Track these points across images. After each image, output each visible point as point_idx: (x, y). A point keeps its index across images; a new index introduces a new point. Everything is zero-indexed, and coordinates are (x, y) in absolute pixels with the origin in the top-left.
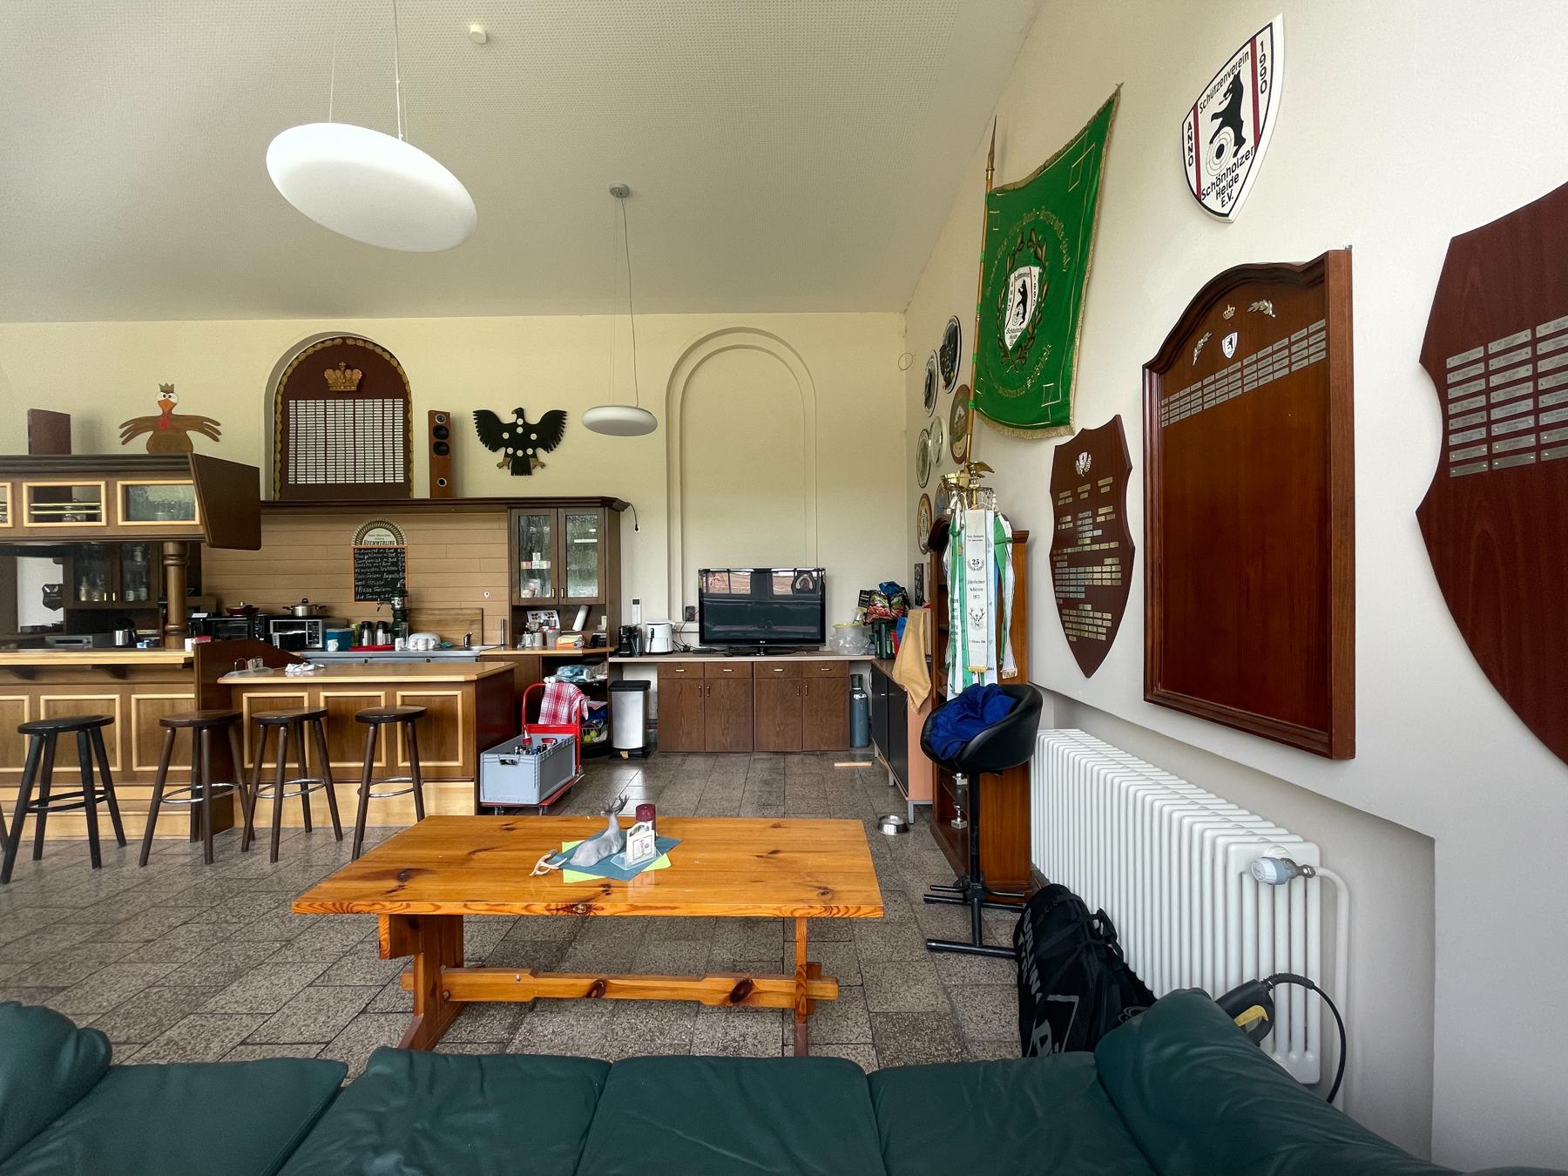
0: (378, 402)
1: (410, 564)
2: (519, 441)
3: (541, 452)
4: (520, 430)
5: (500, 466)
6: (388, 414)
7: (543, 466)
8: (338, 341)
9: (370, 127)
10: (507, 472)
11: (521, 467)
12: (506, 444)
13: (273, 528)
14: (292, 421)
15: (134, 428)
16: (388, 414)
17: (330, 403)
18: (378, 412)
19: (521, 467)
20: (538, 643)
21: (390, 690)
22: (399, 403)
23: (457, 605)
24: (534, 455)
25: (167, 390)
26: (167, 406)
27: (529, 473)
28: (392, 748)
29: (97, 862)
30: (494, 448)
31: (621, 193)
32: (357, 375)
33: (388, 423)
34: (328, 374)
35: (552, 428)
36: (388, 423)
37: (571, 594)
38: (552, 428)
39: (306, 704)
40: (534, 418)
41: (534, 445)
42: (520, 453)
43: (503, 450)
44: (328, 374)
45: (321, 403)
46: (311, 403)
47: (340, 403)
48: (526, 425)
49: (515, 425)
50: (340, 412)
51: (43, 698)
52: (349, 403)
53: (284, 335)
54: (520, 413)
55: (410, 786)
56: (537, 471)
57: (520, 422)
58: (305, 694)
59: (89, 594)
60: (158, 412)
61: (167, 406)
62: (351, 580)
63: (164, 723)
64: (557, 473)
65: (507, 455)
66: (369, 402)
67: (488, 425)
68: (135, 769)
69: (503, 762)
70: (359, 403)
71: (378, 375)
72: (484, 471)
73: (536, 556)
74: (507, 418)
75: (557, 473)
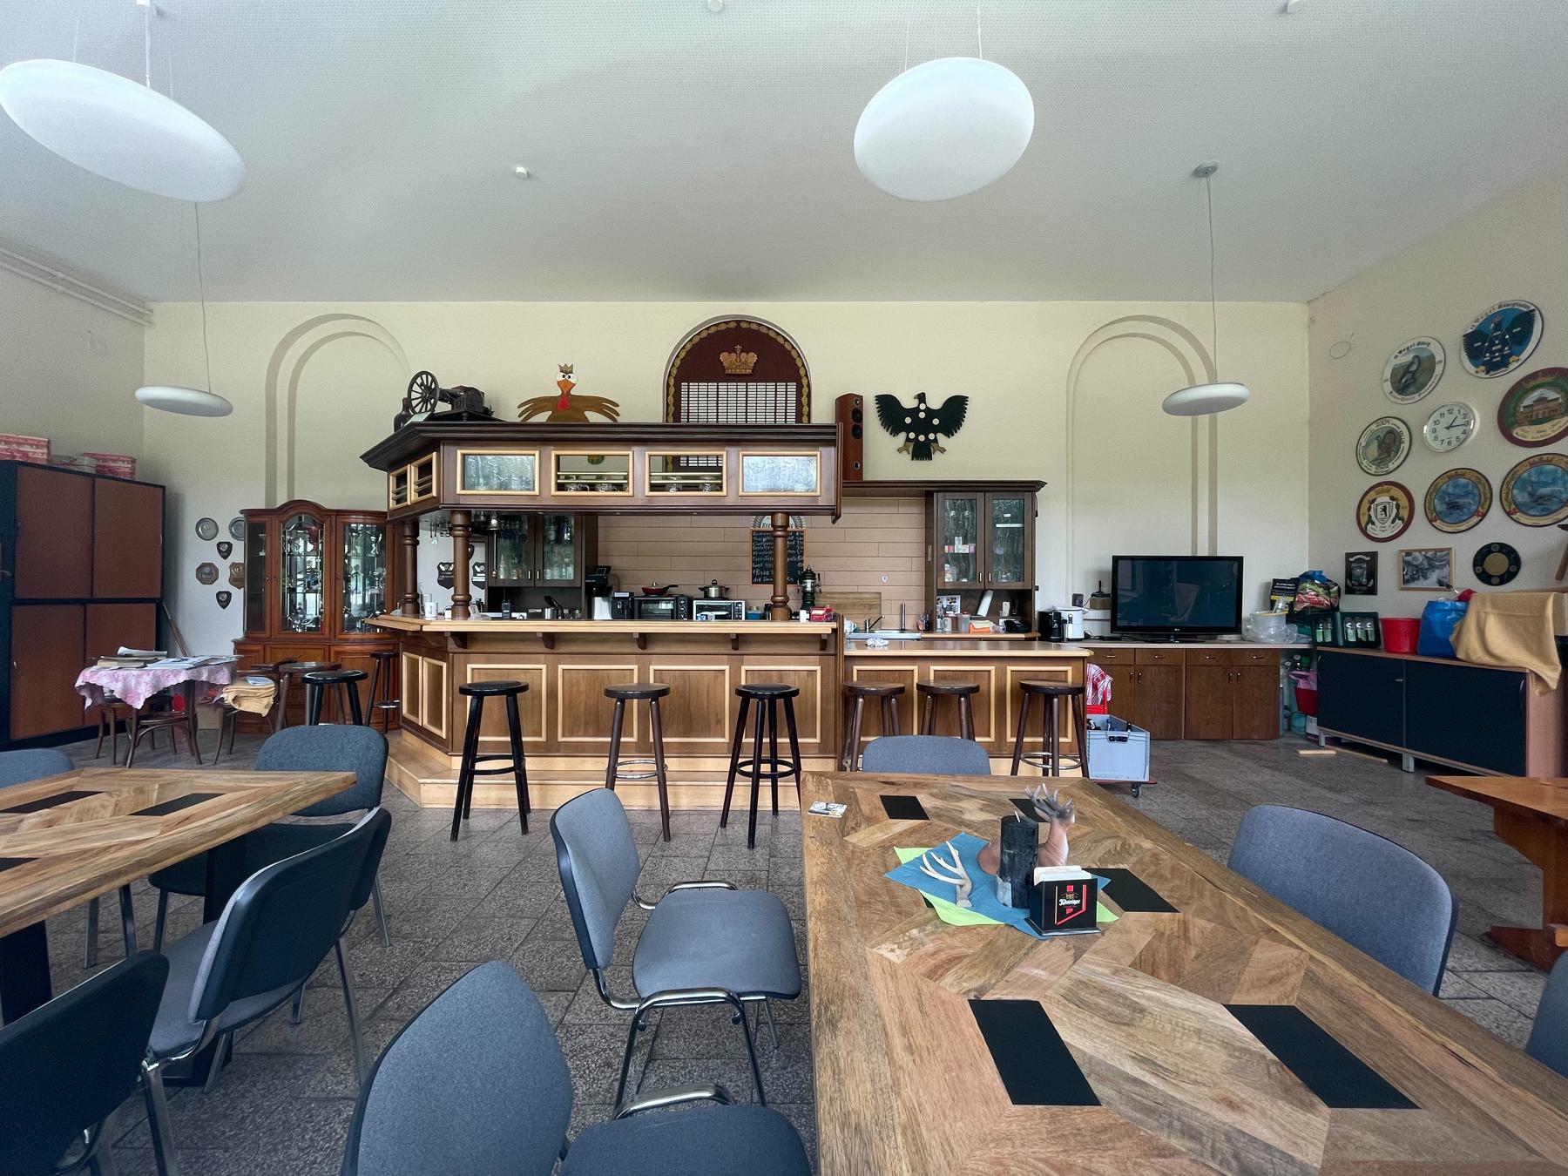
0: (771, 386)
1: (808, 547)
2: (922, 426)
3: (940, 436)
4: (922, 415)
5: (900, 450)
6: (781, 397)
7: (943, 450)
8: (733, 325)
9: (189, 108)
10: (906, 457)
11: (922, 452)
12: (908, 429)
13: (853, 510)
14: (684, 403)
15: (537, 405)
16: (781, 397)
17: (723, 386)
18: (771, 395)
19: (922, 452)
20: (948, 628)
21: (1000, 664)
22: (792, 387)
23: (855, 589)
24: (936, 440)
25: (567, 371)
26: (566, 386)
27: (930, 458)
28: (1000, 727)
29: (724, 823)
30: (895, 432)
31: (1203, 172)
32: (752, 358)
33: (781, 405)
34: (724, 357)
35: (953, 413)
36: (781, 405)
37: (548, 577)
38: (953, 413)
39: (1070, 679)
40: (935, 402)
41: (936, 430)
42: (922, 438)
43: (903, 435)
44: (724, 357)
45: (713, 386)
46: (703, 386)
47: (732, 386)
48: (927, 410)
49: (917, 410)
50: (761, 395)
51: (561, 667)
52: (742, 386)
53: (693, 314)
54: (921, 398)
55: (510, 763)
56: (936, 456)
57: (922, 407)
58: (915, 668)
59: (508, 571)
60: (557, 392)
61: (566, 386)
62: (747, 563)
63: (609, 693)
64: (957, 458)
65: (908, 440)
66: (761, 386)
67: (890, 409)
68: (561, 739)
69: (1112, 739)
70: (752, 386)
71: (775, 358)
72: (886, 455)
73: (958, 541)
74: (908, 402)
75: (957, 458)
